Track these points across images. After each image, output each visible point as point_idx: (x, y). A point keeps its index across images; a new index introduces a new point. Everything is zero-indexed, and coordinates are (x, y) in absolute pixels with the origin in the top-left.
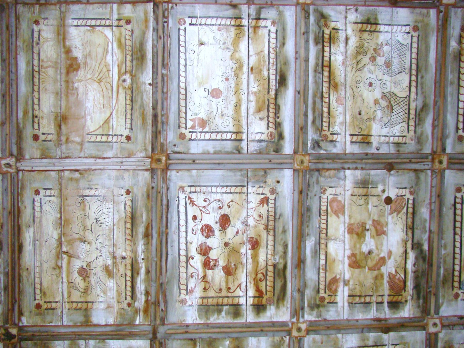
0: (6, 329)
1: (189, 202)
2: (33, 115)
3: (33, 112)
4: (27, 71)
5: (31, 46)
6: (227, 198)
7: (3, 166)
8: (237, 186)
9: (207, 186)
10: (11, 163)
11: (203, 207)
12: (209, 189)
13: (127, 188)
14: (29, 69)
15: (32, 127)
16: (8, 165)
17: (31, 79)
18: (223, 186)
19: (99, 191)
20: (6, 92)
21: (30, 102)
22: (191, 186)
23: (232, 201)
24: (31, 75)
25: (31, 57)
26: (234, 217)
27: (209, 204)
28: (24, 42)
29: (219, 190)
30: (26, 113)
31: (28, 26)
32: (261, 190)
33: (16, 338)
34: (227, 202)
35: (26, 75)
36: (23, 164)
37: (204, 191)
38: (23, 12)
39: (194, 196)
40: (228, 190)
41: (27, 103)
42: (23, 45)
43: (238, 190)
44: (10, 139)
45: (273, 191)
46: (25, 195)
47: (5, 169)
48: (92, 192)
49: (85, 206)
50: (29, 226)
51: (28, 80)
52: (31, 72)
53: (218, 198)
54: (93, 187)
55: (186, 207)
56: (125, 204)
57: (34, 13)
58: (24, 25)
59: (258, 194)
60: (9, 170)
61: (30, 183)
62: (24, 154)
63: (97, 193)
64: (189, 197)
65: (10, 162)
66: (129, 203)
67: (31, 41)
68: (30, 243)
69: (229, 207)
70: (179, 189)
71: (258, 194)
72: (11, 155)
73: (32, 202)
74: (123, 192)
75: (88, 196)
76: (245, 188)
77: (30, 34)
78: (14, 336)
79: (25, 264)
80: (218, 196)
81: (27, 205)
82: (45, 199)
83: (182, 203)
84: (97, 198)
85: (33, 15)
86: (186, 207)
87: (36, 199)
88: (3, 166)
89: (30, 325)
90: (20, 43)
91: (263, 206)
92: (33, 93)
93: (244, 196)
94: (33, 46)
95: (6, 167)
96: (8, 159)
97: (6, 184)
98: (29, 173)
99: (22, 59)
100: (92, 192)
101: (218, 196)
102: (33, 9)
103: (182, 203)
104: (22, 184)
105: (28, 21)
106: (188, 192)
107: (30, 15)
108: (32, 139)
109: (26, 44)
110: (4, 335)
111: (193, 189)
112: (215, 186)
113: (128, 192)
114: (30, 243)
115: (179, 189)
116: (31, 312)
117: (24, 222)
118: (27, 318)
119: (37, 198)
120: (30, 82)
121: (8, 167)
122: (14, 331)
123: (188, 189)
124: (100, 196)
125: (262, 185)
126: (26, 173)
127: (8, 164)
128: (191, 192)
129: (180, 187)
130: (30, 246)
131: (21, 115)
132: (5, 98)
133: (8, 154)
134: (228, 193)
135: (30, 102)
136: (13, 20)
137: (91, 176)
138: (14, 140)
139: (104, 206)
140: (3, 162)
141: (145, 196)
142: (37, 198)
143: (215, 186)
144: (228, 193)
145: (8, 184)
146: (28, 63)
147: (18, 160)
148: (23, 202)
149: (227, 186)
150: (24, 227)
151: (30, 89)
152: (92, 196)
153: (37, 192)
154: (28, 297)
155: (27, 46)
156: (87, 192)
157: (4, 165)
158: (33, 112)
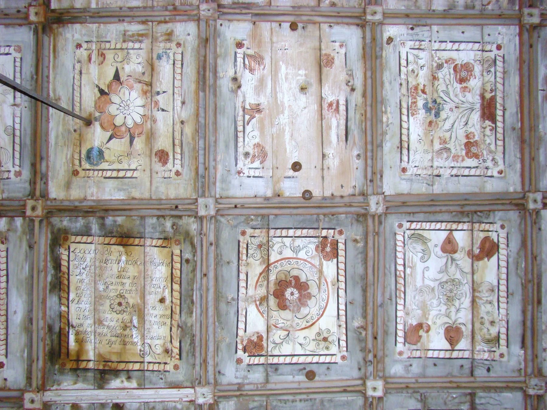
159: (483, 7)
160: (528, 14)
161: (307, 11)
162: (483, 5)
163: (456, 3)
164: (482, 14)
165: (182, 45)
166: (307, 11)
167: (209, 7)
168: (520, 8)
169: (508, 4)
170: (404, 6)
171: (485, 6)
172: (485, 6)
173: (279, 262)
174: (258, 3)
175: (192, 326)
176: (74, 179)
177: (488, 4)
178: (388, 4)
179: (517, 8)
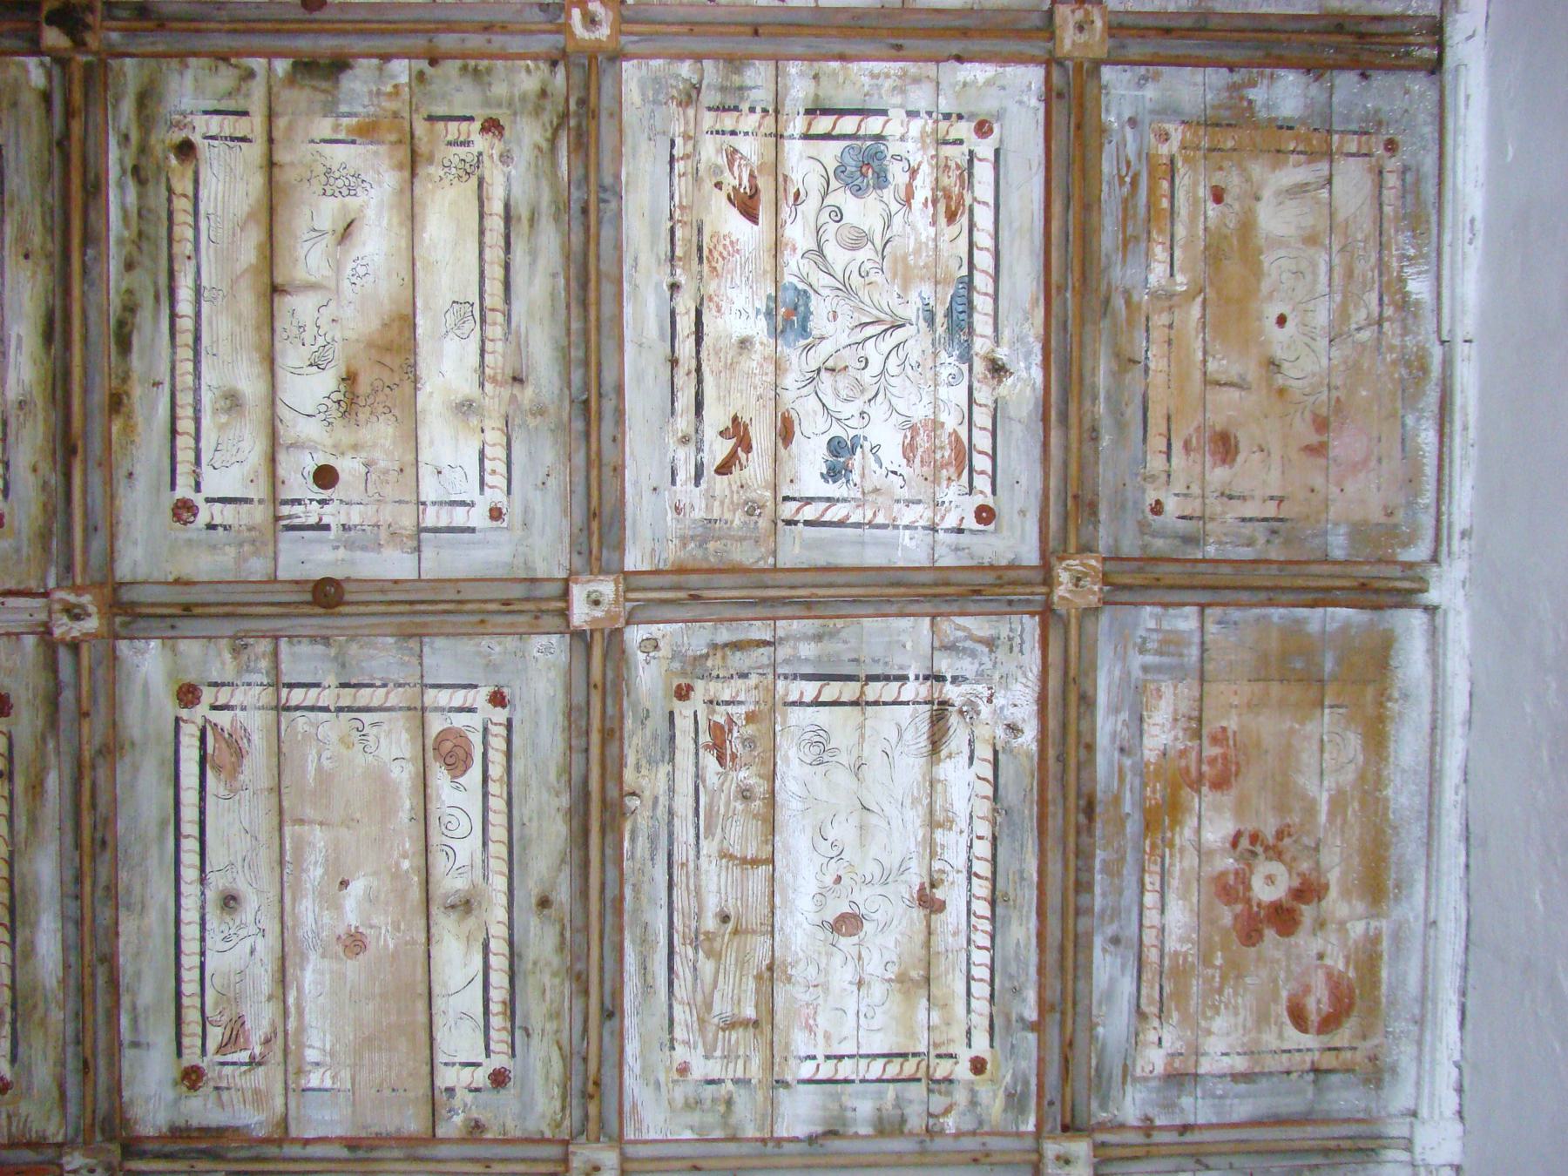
0: (79, 44)
2: (11, 779)
3: (11, 792)
4: (34, 925)
5: (20, 1008)
7: (92, 609)
10: (65, 619)
14: (28, 932)
15: (15, 740)
16: (75, 613)
17: (18, 898)
20: (93, 858)
21: (22, 823)
24: (19, 910)
25: (18, 971)
26: (815, 412)
28: (43, 1023)
30: (36, 788)
31: (30, 1072)
33: (44, 13)
35: (37, 913)
36: (26, 616)
38: (49, 1119)
41: (33, 821)
42: (47, 1010)
44: (78, 699)
46: (35, 509)
47: (86, 599)
50: (21, 404)
51: (31, 898)
52: (18, 924)
57: (9, 1117)
58: (43, 1074)
60: (72, 598)
61: (18, 550)
62: (41, 649)
65: (70, 624)
67: (19, 1024)
68: (19, 347)
69: (1225, 446)
72: (75, 646)
73: (12, 487)
77: (22, 1049)
78: (51, 20)
79: (34, 273)
81: (31, 478)
82: (470, 491)
85: (11, 1108)
88: (92, 609)
89: (17, 59)
90: (56, 1015)
92: (12, 853)
94: (14, 1007)
95: (82, 607)
96: (75, 633)
97: (98, 544)
98: (22, 587)
99: (51, 966)
102: (14, 1129)
104: (46, 549)
105: (29, 1088)
107: (25, 1108)
108: (12, 700)
109: (37, 1016)
110: (87, 27)
114: (19, 347)
116: (15, 104)
117: (40, 417)
118: (28, 81)
119: (497, 496)
120: (23, 891)
121: (75, 606)
122: (53, 37)
126: (33, 584)
127: (77, 618)
130: (19, 337)
131: (52, 781)
132: (99, 835)
133: (85, 648)
135: (22, 823)
136: (72, 1091)
138: (67, 696)
140: (92, 624)
142: (497, 496)
145: (86, 550)
146: (30, 951)
147: (45, 632)
148: (45, 486)
150: (39, 401)
151: (22, 866)
154: (24, 155)
155: (35, 1006)
157: (89, 615)
158: (11, 792)
159: (931, 1121)
160: (1058, 1158)
161: (397, 1160)
162: (930, 1115)
163: (849, 1114)
164: (923, 1152)
165: (495, 524)
166: (397, 1160)
167: (91, 1162)
168: (1038, 1134)
169: (1005, 1110)
170: (692, 1128)
171: (937, 1116)
172: (937, 1116)
173: (1434, 255)
174: (248, 1126)
175: (1347, 221)
176: (670, 280)
177: (947, 1111)
178: (641, 1122)
179: (1030, 1126)
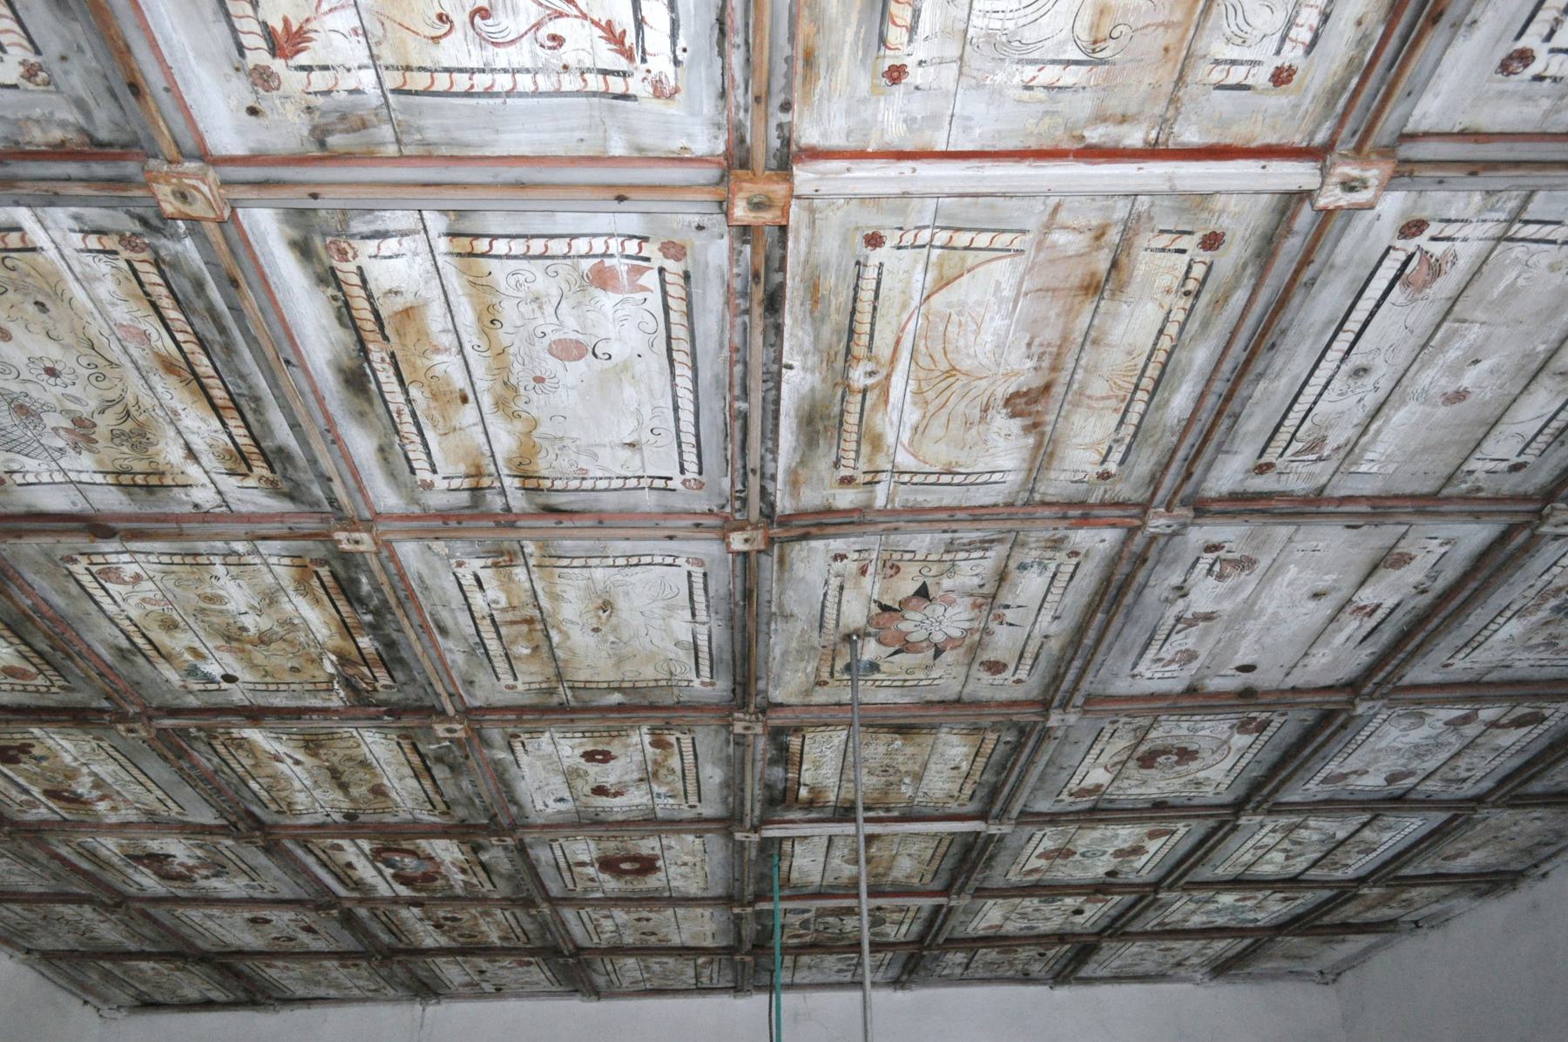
1: (630, 40)
6: (458, 49)
8: (426, 93)
9: (558, 93)
11: (561, 15)
12: (544, 83)
13: (899, 90)
18: (488, 93)
19: (1017, 80)
22: (625, 97)
23: (436, 39)
27: (537, 26)
29: (503, 82)
32: (319, 80)
34: (457, 35)
37: (565, 78)
39: (608, 57)
40: (462, 82)
43: (419, 81)
45: (263, 78)
48: (1050, 74)
49: (1095, 26)
53: (501, 51)
54: (1041, 94)
55: (639, 23)
56: (912, 30)
59: (325, 68)
63: (1030, 71)
64: (631, 58)
66: (896, 35)
70: (677, 90)
71: (325, 68)
74: (915, 76)
75: (1069, 63)
76: (388, 85)
80: (502, 57)
83: (658, 38)
84: (1035, 55)
86: (639, 23)
87: (1300, 51)
91: (286, 21)
93: (387, 56)
100: (1050, 74)
101: (502, 57)
103: (658, 38)
106: (638, 76)
111: (617, 85)
112: (522, 95)
113: (896, 74)
115: (677, 90)
123: (635, 85)
124: (1020, 61)
125: (320, 101)
128: (624, 74)
129: (671, 96)
134: (461, 70)
137: (1043, 127)
139: (1010, 25)
141: (822, 62)
142: (1292, 55)
143: (522, 95)
144: (461, 70)
149: (468, 94)
152: (1053, 62)
153: (1281, 77)
156: (1070, 76)
